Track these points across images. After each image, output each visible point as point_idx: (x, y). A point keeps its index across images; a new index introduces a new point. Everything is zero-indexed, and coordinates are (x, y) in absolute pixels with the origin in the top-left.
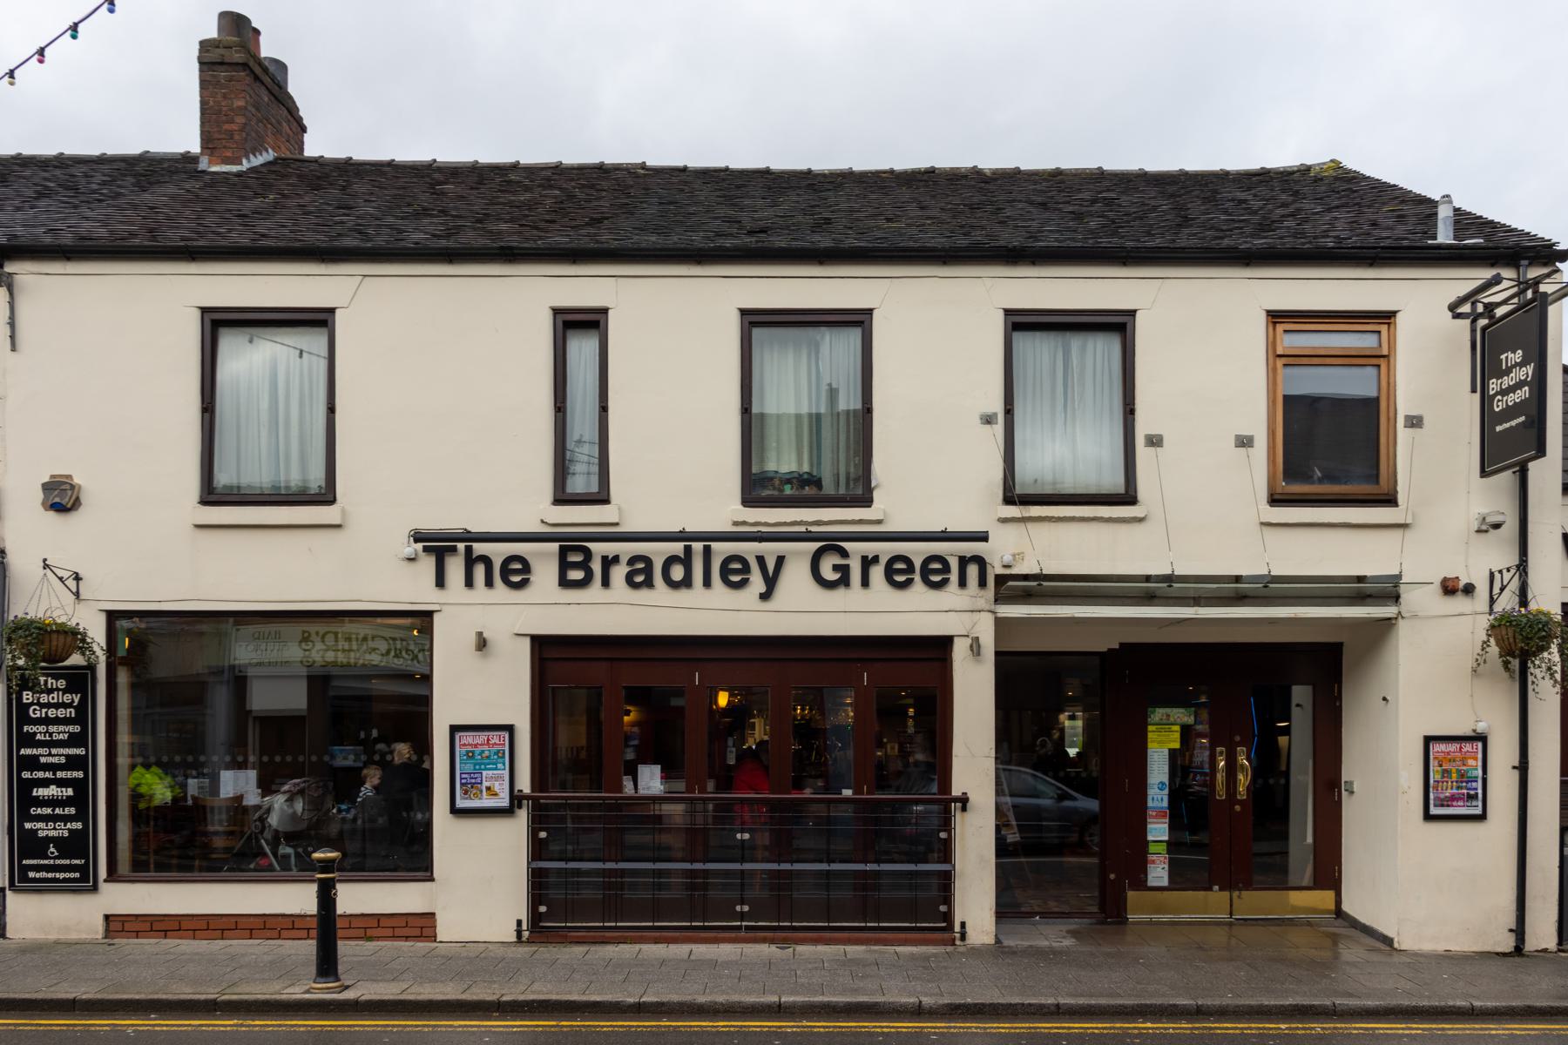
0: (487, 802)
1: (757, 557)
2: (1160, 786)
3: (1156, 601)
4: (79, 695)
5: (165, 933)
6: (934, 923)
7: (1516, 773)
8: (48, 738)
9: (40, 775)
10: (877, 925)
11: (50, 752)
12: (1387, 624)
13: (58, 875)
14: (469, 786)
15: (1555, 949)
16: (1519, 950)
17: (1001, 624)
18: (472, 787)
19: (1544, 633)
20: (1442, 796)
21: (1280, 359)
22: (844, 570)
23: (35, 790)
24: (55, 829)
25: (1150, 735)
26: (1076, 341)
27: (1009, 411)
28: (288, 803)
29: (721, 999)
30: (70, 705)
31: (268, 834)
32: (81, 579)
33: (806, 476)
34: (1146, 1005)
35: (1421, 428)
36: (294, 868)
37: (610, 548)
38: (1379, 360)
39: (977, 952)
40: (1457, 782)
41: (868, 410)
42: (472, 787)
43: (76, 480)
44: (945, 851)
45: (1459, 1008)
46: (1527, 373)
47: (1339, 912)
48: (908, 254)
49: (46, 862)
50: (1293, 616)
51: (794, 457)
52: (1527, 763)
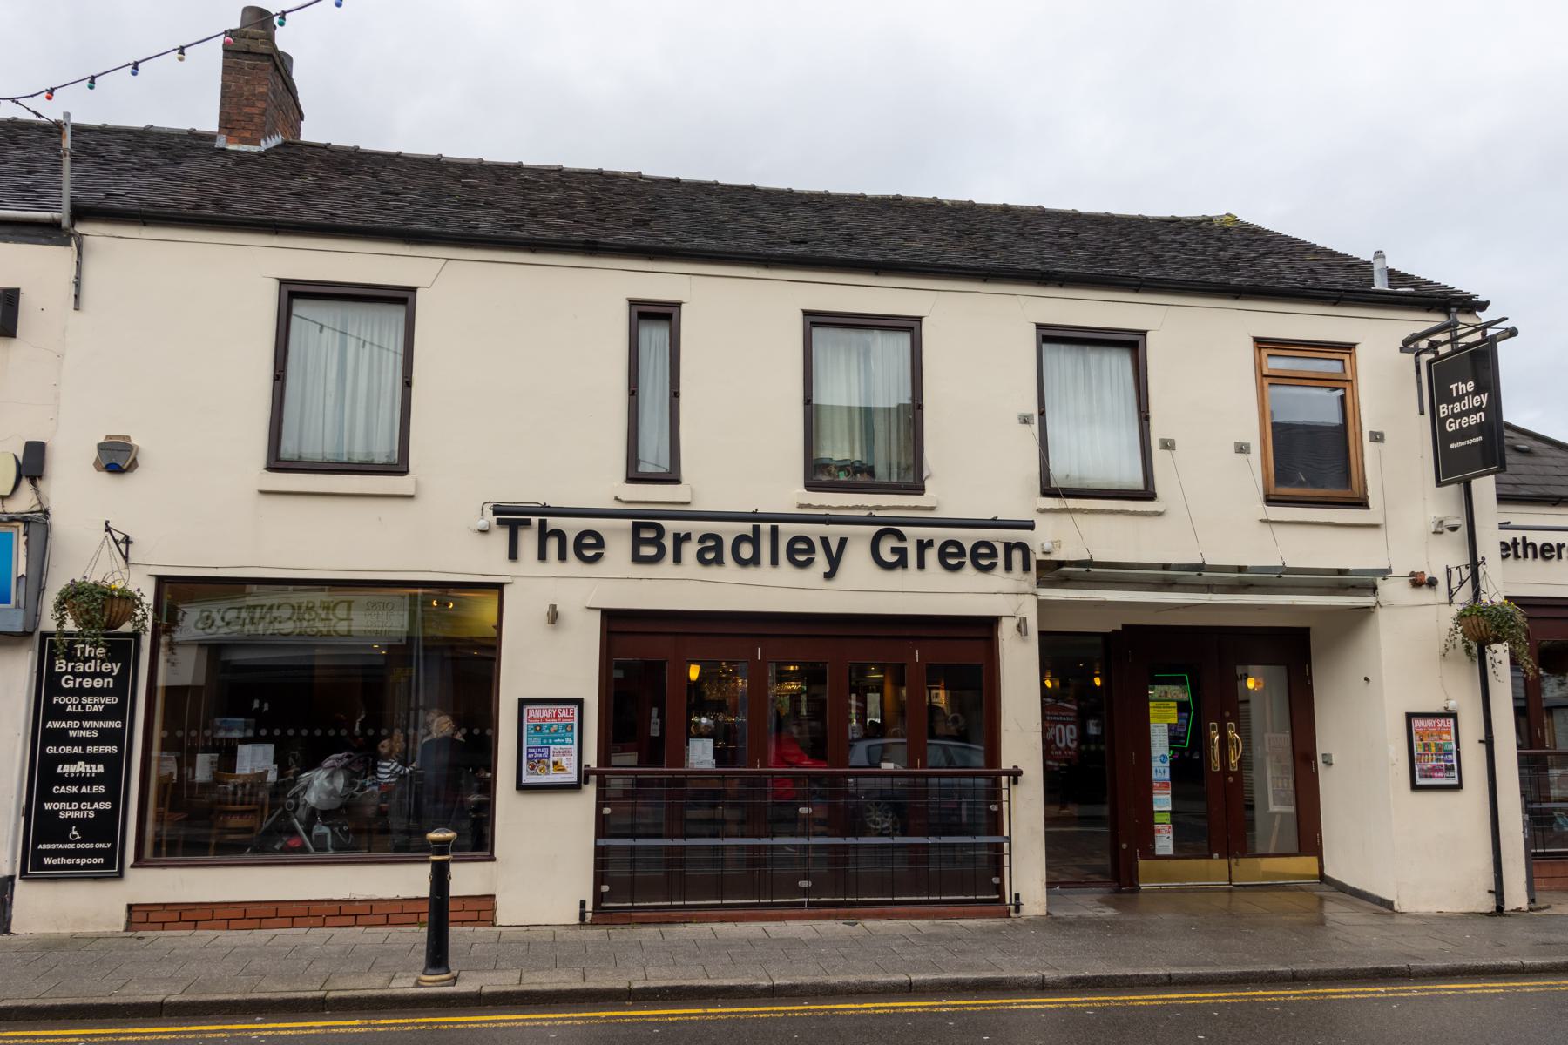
0: (553, 777)
1: (821, 538)
2: (1162, 758)
3: (1175, 587)
4: (119, 664)
5: (195, 924)
6: (988, 895)
7: (1483, 748)
8: (80, 710)
9: (68, 750)
10: (720, 902)
11: (81, 724)
12: (1367, 611)
13: (78, 861)
14: (536, 761)
15: (1527, 909)
16: (1500, 909)
17: (1043, 605)
18: (539, 762)
19: (1512, 623)
20: (1425, 767)
21: (1268, 380)
22: (901, 553)
23: (60, 766)
24: (79, 809)
25: (1152, 711)
26: (1094, 356)
27: (1042, 413)
28: (328, 779)
29: (852, 979)
30: (108, 675)
31: (302, 813)
32: (132, 542)
33: (857, 464)
34: (1248, 973)
35: (1383, 442)
36: (330, 848)
37: (925, 533)
38: (1342, 384)
39: (1033, 922)
40: (1436, 755)
41: (917, 405)
42: (539, 762)
43: (134, 442)
44: (994, 823)
45: (1513, 966)
46: (1481, 401)
47: (1322, 878)
48: (955, 271)
49: (66, 846)
50: (1291, 603)
51: (846, 446)
52: (1492, 737)
